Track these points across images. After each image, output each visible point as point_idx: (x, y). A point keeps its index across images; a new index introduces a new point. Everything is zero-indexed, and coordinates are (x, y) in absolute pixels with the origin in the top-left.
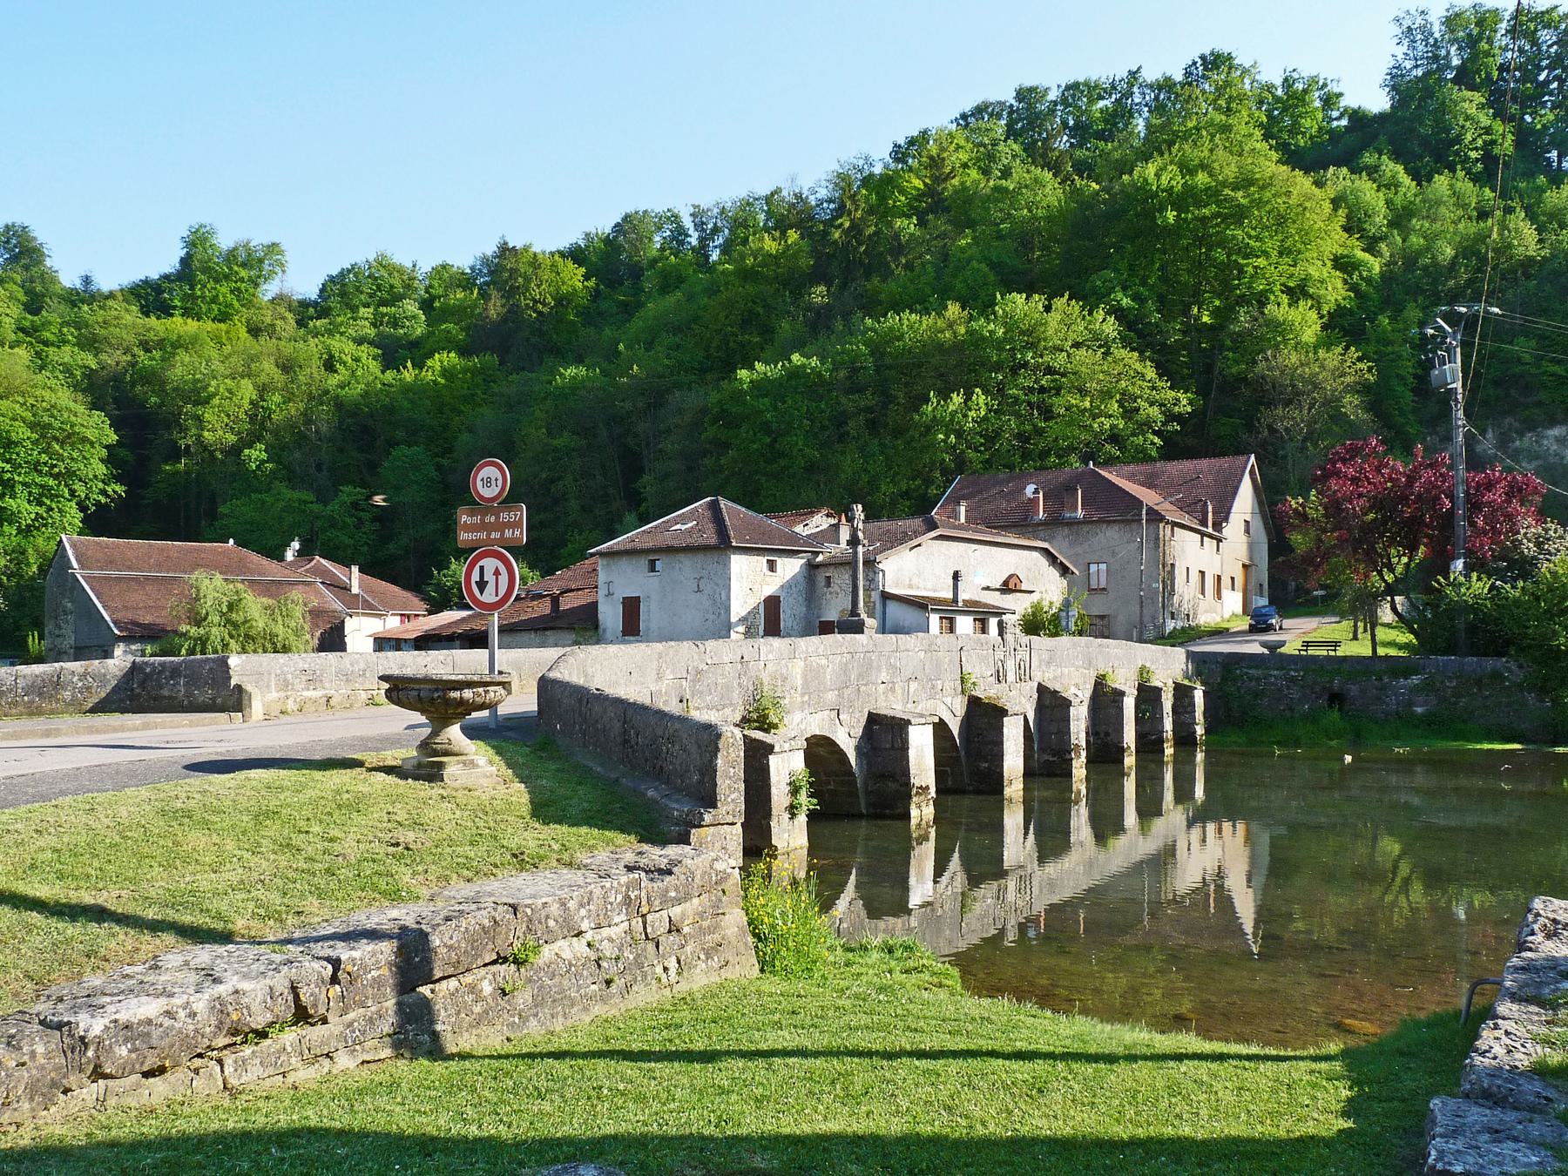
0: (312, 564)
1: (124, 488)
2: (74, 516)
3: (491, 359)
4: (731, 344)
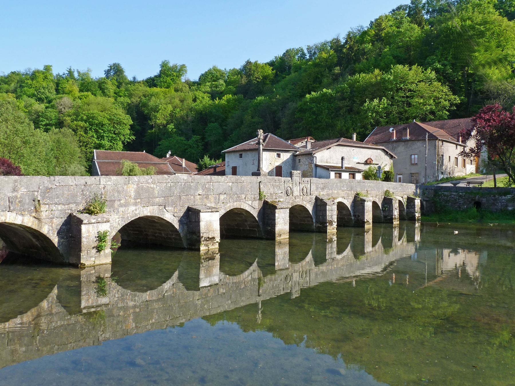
0: (174, 157)
1: (135, 137)
2: (120, 145)
3: (241, 96)
4: (310, 87)
